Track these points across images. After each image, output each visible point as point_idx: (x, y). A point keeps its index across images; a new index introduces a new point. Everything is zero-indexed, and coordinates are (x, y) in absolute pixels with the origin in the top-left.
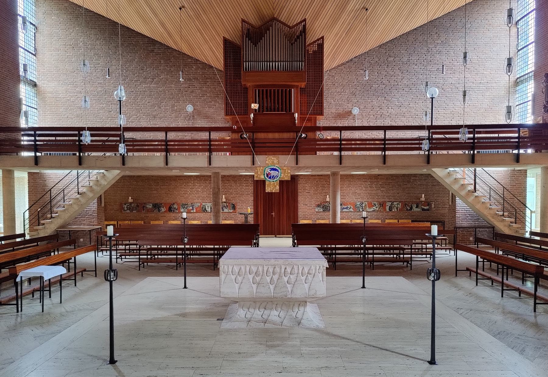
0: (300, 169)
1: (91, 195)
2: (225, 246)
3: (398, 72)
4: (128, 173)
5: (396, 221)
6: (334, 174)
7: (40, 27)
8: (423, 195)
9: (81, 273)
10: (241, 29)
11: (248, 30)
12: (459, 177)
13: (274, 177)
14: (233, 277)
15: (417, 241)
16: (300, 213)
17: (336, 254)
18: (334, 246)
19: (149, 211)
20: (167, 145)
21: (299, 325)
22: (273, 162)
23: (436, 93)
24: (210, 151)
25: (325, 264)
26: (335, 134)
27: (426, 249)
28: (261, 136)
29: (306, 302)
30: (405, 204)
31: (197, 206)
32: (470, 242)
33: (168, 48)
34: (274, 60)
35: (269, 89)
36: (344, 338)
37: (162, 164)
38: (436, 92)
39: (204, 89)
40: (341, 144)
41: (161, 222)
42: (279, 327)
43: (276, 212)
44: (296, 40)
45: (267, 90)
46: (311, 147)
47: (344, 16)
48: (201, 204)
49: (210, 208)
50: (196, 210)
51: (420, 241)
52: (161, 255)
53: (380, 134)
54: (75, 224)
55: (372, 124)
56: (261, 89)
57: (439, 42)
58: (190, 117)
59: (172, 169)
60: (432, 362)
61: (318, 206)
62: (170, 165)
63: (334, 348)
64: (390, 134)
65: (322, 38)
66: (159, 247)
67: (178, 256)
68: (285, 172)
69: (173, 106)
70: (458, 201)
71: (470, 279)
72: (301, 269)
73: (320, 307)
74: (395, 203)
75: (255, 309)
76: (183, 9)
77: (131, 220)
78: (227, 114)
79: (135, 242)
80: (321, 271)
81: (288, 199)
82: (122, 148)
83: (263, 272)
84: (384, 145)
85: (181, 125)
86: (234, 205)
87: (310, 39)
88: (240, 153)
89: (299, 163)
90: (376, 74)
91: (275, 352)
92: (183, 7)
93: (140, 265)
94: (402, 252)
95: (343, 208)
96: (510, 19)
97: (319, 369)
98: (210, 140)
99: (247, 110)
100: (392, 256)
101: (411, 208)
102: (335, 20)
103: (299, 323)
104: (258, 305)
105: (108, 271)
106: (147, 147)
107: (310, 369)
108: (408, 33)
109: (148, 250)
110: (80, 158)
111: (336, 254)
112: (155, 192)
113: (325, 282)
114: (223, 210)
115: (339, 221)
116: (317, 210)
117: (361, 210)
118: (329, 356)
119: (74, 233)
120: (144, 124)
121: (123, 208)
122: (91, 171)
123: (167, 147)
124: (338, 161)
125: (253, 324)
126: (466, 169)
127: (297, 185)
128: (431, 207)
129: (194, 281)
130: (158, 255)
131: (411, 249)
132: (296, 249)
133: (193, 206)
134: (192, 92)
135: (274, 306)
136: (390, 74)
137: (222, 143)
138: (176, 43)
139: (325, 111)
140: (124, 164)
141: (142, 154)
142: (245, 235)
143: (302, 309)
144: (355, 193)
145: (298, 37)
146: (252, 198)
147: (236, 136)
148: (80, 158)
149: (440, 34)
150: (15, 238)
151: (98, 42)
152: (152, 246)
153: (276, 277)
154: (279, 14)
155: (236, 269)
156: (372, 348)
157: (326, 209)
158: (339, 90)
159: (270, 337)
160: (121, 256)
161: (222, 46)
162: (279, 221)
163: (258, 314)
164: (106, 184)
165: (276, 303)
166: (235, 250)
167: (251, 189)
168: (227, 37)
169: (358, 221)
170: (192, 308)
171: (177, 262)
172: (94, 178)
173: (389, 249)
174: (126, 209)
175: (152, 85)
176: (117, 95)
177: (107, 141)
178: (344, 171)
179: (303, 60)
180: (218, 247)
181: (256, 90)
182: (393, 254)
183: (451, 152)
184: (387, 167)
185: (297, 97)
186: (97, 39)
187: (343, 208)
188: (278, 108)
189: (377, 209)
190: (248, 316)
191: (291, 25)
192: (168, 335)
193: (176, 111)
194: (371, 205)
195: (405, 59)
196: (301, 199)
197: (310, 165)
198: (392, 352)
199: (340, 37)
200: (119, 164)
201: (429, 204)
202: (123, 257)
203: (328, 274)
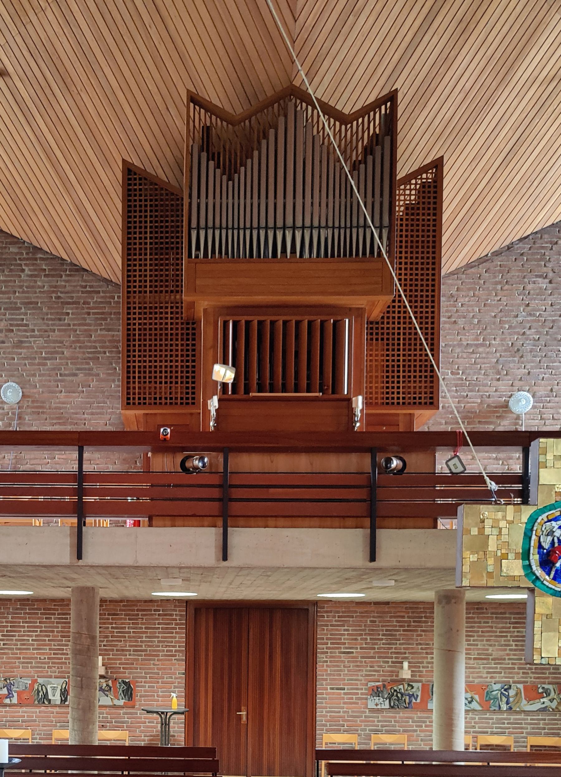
11: (207, 130)
16: (323, 714)
24: (81, 511)
28: (250, 463)
31: (22, 688)
39: (55, 336)
49: (58, 693)
58: (12, 419)
61: (377, 692)
87: (410, 158)
88: (179, 521)
89: (381, 553)
98: (81, 476)
102: (480, 104)
116: (371, 705)
117: (504, 707)
127: (314, 633)
133: (9, 687)
134: (19, 344)
150: (155, 583)
167: (179, 639)
181: (226, 324)
185: (359, 346)
191: (346, 111)
196: (325, 669)
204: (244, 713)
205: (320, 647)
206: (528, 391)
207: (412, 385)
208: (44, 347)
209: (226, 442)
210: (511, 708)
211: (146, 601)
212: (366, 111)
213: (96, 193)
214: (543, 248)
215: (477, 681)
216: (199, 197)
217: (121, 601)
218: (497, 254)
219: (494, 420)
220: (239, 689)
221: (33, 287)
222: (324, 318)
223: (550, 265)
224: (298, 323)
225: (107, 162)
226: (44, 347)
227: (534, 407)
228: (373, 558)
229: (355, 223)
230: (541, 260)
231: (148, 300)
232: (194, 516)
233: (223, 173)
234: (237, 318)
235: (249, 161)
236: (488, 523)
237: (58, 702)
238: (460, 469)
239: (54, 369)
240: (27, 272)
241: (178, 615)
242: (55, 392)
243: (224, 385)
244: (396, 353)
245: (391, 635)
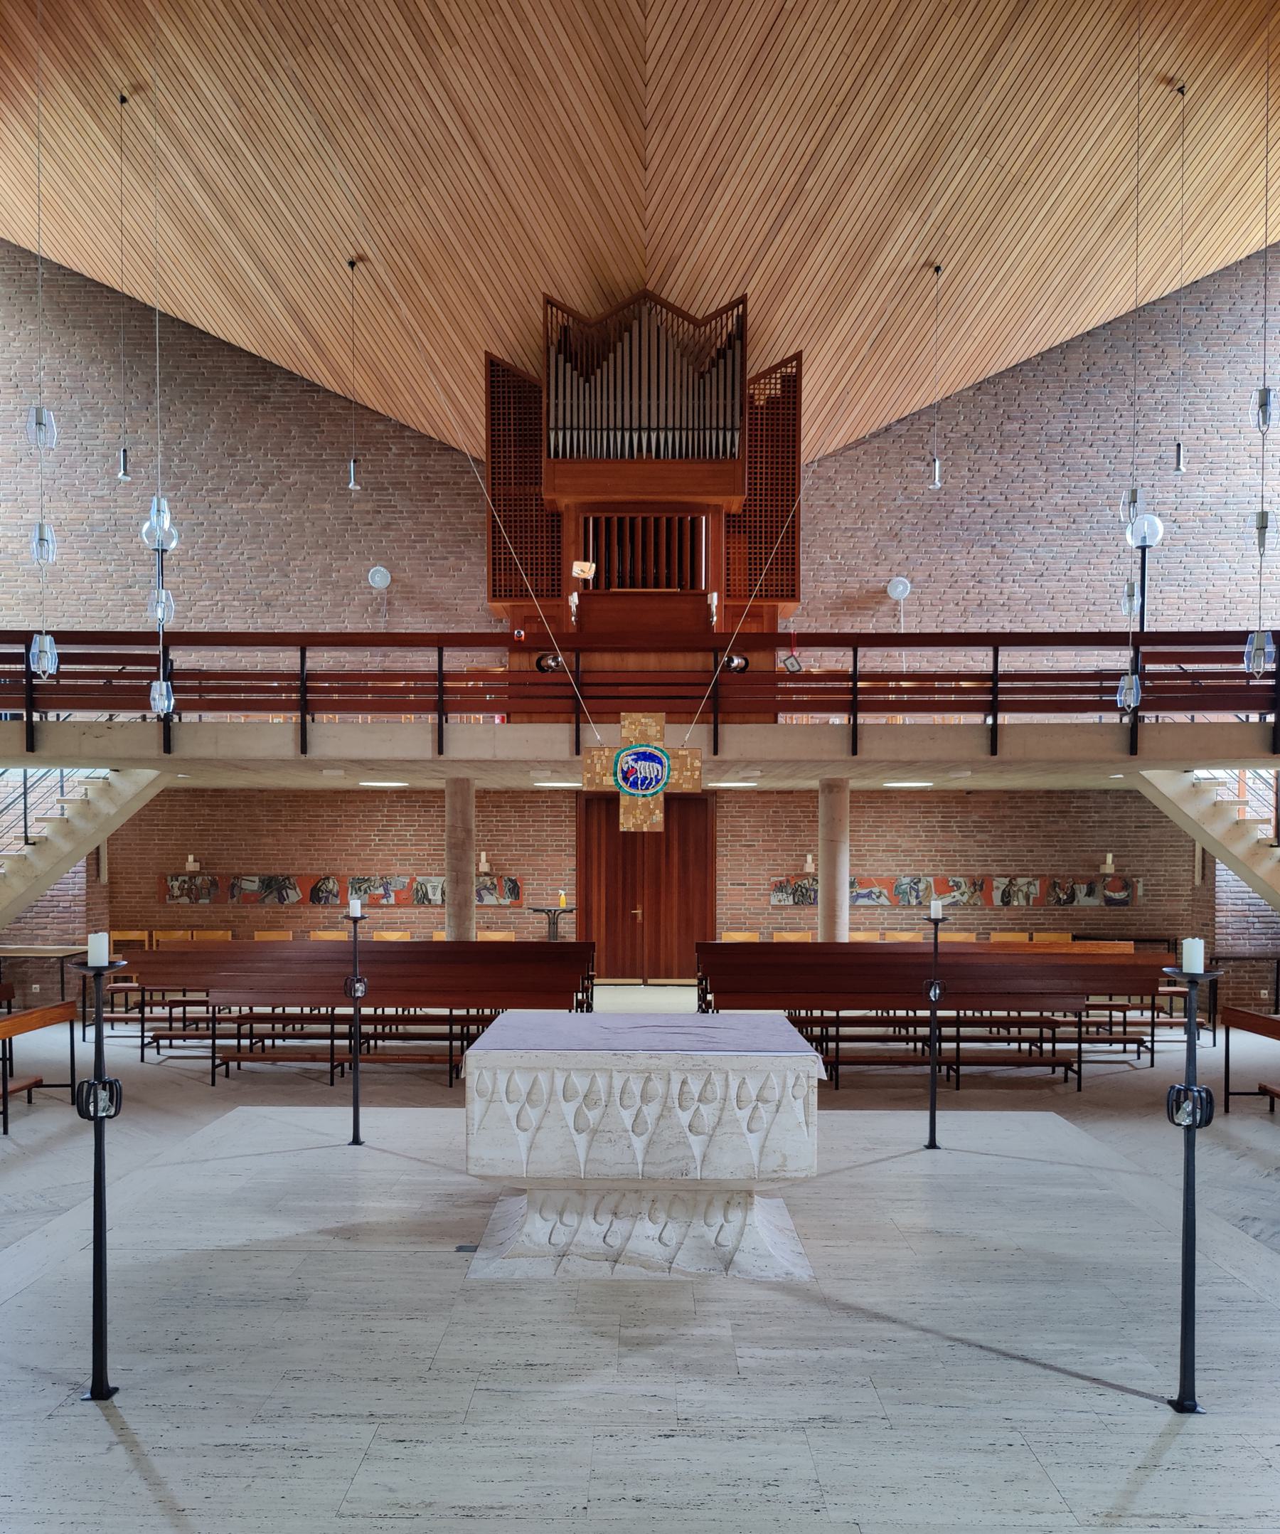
0: (723, 768)
1: (65, 846)
2: (487, 1012)
3: (1034, 468)
4: (183, 780)
5: (1023, 937)
6: (832, 787)
8: (1110, 857)
9: (25, 1093)
10: (541, 328)
11: (565, 329)
12: (1226, 798)
13: (646, 783)
14: (511, 1110)
15: (1094, 1000)
16: (723, 911)
17: (838, 1038)
18: (833, 1014)
19: (248, 898)
20: (304, 690)
21: (726, 1269)
22: (643, 734)
23: (1155, 534)
24: (442, 709)
25: (813, 1066)
26: (837, 659)
27: (1125, 1023)
28: (604, 661)
29: (750, 1194)
31: (399, 887)
32: (1260, 1003)
33: (313, 388)
34: (645, 424)
35: (627, 516)
36: (878, 1317)
37: (287, 746)
38: (1155, 528)
39: (425, 517)
41: (289, 936)
42: (659, 1275)
43: (647, 901)
44: (714, 363)
45: (621, 520)
46: (762, 698)
47: (865, 291)
48: (413, 880)
49: (439, 892)
50: (397, 899)
51: (1103, 1000)
52: (284, 1037)
53: (978, 660)
54: (14, 938)
56: (603, 516)
57: (1165, 372)
58: (381, 604)
59: (320, 765)
60: (1185, 1404)
61: (780, 887)
62: (315, 751)
63: (847, 1352)
64: (1014, 660)
65: (798, 356)
66: (279, 1010)
67: (337, 1042)
68: (684, 765)
69: (327, 571)
70: (1224, 874)
71: (1272, 1121)
72: (734, 1085)
73: (793, 1210)
74: (1021, 881)
75: (581, 1214)
76: (360, 265)
77: (192, 928)
78: (495, 595)
79: (201, 996)
80: (801, 1092)
82: (161, 698)
83: (610, 1094)
84: (992, 693)
85: (350, 628)
86: (514, 882)
87: (758, 362)
88: (535, 717)
90: (965, 472)
91: (648, 1362)
92: (362, 258)
93: (214, 1067)
94: (1047, 1033)
95: (859, 896)
96: (1265, 413)
97: (801, 1425)
98: (441, 676)
99: (557, 583)
100: (1014, 1046)
101: (1072, 897)
102: (840, 295)
103: (728, 1264)
104: (591, 1205)
105: (91, 1085)
106: (242, 696)
107: (768, 1423)
108: (1067, 347)
109: (241, 1020)
110: (31, 729)
111: (838, 1038)
112: (270, 840)
113: (813, 1129)
114: (481, 899)
116: (774, 901)
117: (914, 902)
118: (834, 1377)
119: (12, 965)
121: (169, 890)
122: (66, 771)
123: (305, 697)
124: (846, 744)
125: (575, 1266)
126: (1249, 774)
127: (713, 825)
128: (1132, 895)
129: (382, 1121)
130: (273, 1037)
131: (1079, 1024)
132: (711, 1018)
133: (386, 886)
134: (387, 527)
135: (646, 1206)
136: (1009, 475)
137: (481, 684)
138: (335, 372)
139: (805, 588)
140: (167, 748)
141: (227, 717)
142: (552, 974)
143: (736, 1216)
144: (893, 849)
145: (721, 354)
146: (572, 863)
147: (524, 662)
148: (31, 729)
149: (1168, 349)
151: (93, 370)
152: (257, 1010)
153: (650, 1112)
154: (663, 279)
155: (521, 1083)
156: (976, 1351)
157: (803, 896)
158: (846, 522)
159: (632, 1316)
160: (156, 1039)
161: (484, 420)
162: (658, 932)
163: (590, 1231)
164: (114, 813)
165: (651, 1196)
166: (514, 1022)
167: (568, 834)
168: (499, 352)
169: (906, 937)
170: (381, 1207)
171: (332, 1060)
172: (77, 794)
173: (1006, 1023)
174: (177, 892)
175: (260, 505)
176: (150, 534)
177: (120, 675)
178: (863, 776)
179: (737, 424)
180: (463, 1012)
181: (586, 520)
182: (1020, 1040)
183: (1203, 717)
184: (1002, 763)
186: (93, 360)
187: (859, 896)
188: (657, 578)
190: (561, 1238)
191: (699, 316)
192: (295, 1301)
193: (335, 585)
195: (1057, 427)
196: (724, 865)
197: (748, 760)
198: (1045, 1366)
199: (852, 357)
200: (155, 750)
201: (1127, 885)
202: (163, 1042)
203: (824, 1103)
204: (639, 912)
205: (720, 840)
206: (907, 577)
207: (774, 577)
208: (413, 530)
209: (578, 643)
210: (920, 903)
211: (533, 792)
212: (719, 313)
213: (463, 376)
214: (921, 429)
215: (886, 874)
216: (557, 397)
217: (506, 792)
218: (875, 435)
219: (873, 605)
221: (401, 466)
222: (681, 515)
223: (928, 447)
224: (657, 520)
225: (471, 347)
226: (413, 530)
227: (912, 593)
228: (716, 753)
229: (708, 425)
230: (918, 442)
231: (512, 492)
232: (549, 712)
233: (581, 375)
234: (598, 515)
235: (605, 363)
236: (596, 758)
237: (439, 902)
238: (796, 668)
239: (423, 553)
240: (394, 450)
241: (568, 807)
242: (424, 576)
243: (586, 581)
244: (758, 545)
245: (794, 826)
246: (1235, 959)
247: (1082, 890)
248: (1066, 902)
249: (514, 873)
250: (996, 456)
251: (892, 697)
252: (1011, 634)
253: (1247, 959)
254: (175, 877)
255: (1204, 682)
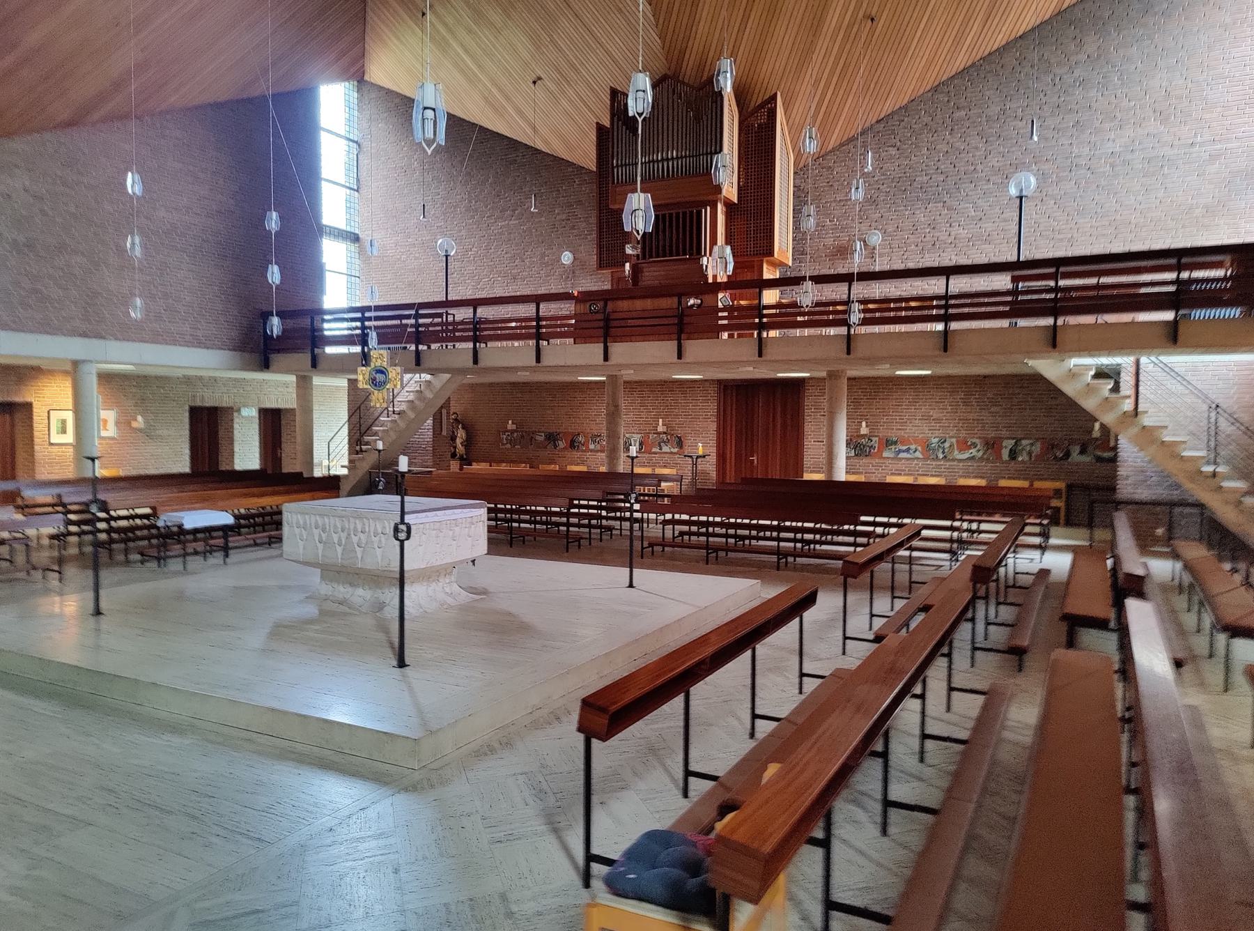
3: (975, 140)
6: (833, 375)
7: (366, 144)
16: (808, 461)
20: (475, 330)
30: (1050, 446)
33: (540, 152)
40: (946, 307)
45: (684, 213)
47: (822, 44)
53: (935, 286)
55: (911, 265)
69: (543, 255)
74: (1024, 442)
81: (784, 426)
84: (947, 308)
92: (540, 78)
115: (841, 475)
120: (499, 292)
121: (501, 440)
134: (573, 228)
144: (926, 418)
146: (714, 426)
148: (417, 352)
167: (712, 408)
177: (432, 324)
188: (664, 250)
189: (981, 454)
194: (964, 445)
195: (994, 110)
199: (827, 87)
220: (752, 441)
223: (898, 138)
241: (713, 392)
246: (1137, 503)
247: (1076, 450)
248: (1061, 459)
249: (680, 432)
250: (948, 137)
251: (892, 314)
252: (868, 273)
253: (1146, 503)
254: (504, 433)
255: (1074, 294)
